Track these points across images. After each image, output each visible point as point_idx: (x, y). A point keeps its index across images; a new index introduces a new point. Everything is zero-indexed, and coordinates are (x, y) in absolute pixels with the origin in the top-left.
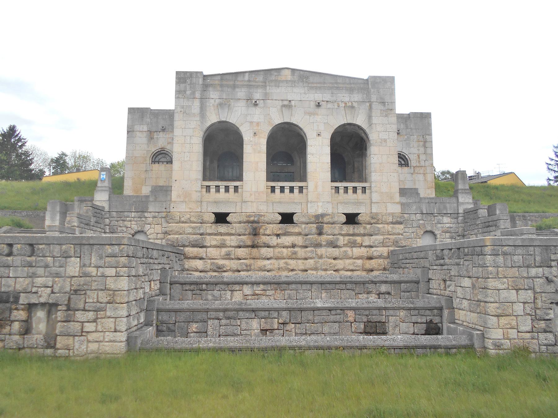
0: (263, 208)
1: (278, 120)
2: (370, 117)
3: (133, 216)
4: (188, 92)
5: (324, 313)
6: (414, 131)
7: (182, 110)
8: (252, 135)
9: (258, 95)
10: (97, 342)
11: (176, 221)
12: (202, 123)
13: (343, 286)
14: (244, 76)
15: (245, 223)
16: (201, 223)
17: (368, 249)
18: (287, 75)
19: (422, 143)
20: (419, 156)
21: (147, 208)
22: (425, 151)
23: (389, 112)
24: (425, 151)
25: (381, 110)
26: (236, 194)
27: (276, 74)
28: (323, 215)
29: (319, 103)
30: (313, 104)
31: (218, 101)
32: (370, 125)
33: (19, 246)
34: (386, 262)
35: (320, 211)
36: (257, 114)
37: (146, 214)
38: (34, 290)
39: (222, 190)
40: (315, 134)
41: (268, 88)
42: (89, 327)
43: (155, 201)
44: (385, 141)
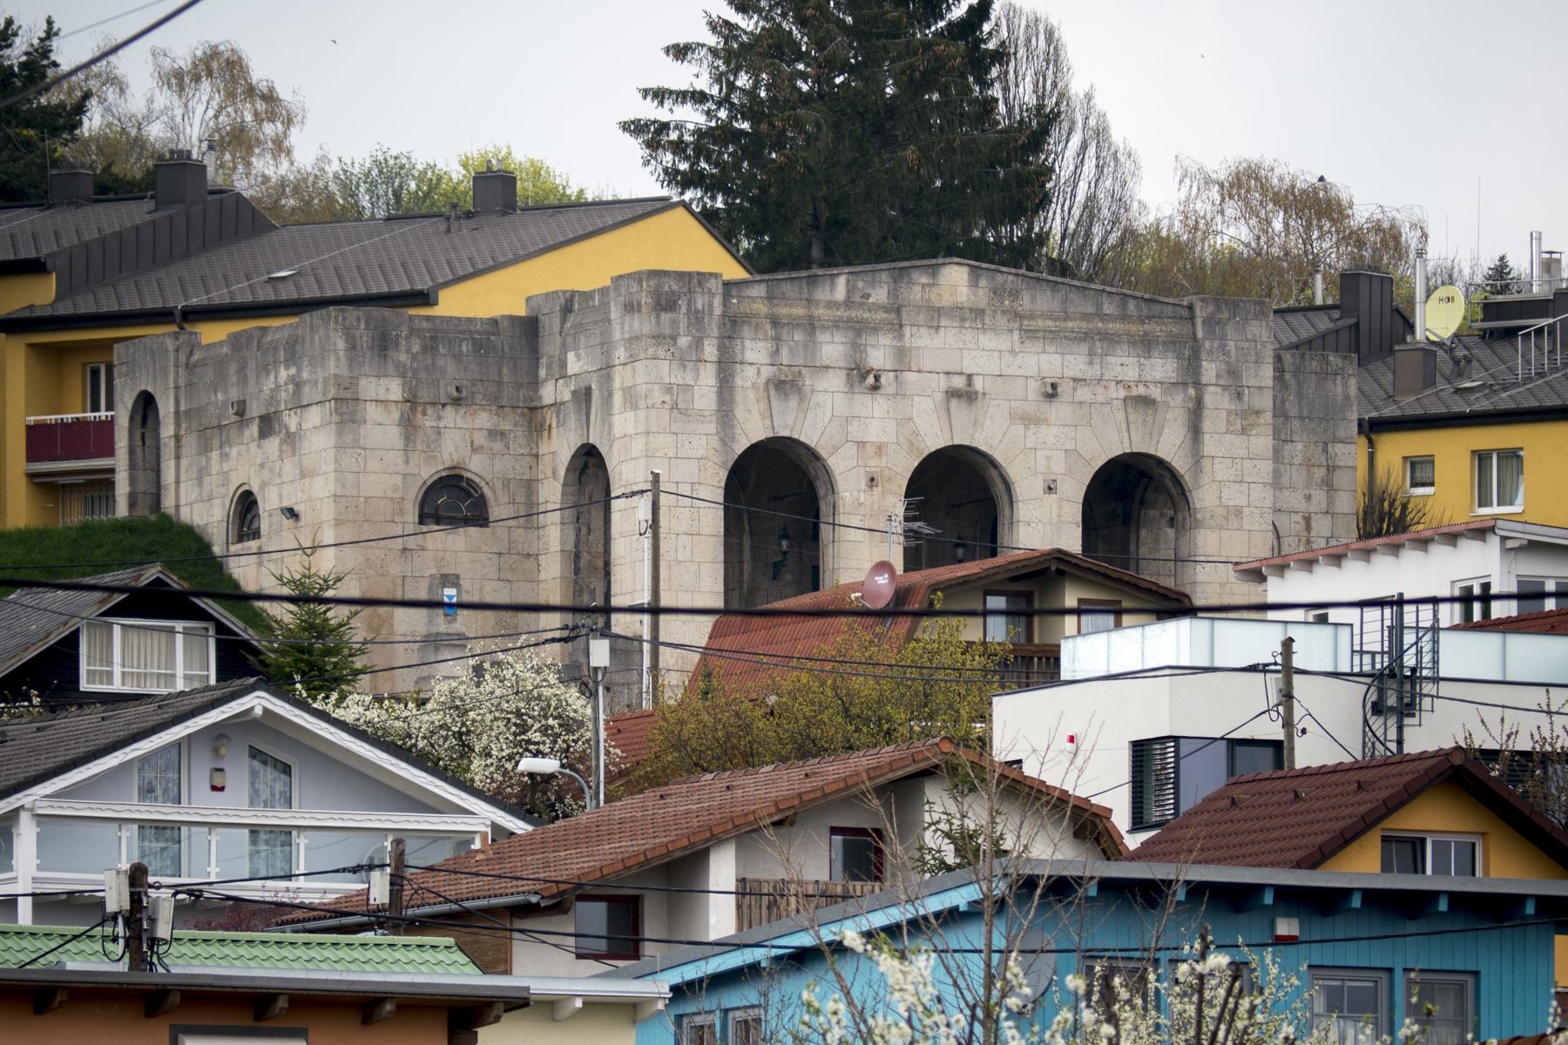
1: (935, 439)
2: (1195, 430)
4: (683, 341)
6: (1296, 424)
7: (667, 398)
8: (863, 486)
9: (879, 355)
12: (723, 442)
19: (1320, 473)
20: (1307, 520)
22: (1330, 502)
23: (1252, 419)
24: (1330, 502)
25: (1229, 413)
27: (924, 280)
29: (1054, 386)
31: (767, 372)
32: (1197, 457)
36: (876, 419)
40: (1039, 486)
41: (907, 331)
44: (1238, 512)
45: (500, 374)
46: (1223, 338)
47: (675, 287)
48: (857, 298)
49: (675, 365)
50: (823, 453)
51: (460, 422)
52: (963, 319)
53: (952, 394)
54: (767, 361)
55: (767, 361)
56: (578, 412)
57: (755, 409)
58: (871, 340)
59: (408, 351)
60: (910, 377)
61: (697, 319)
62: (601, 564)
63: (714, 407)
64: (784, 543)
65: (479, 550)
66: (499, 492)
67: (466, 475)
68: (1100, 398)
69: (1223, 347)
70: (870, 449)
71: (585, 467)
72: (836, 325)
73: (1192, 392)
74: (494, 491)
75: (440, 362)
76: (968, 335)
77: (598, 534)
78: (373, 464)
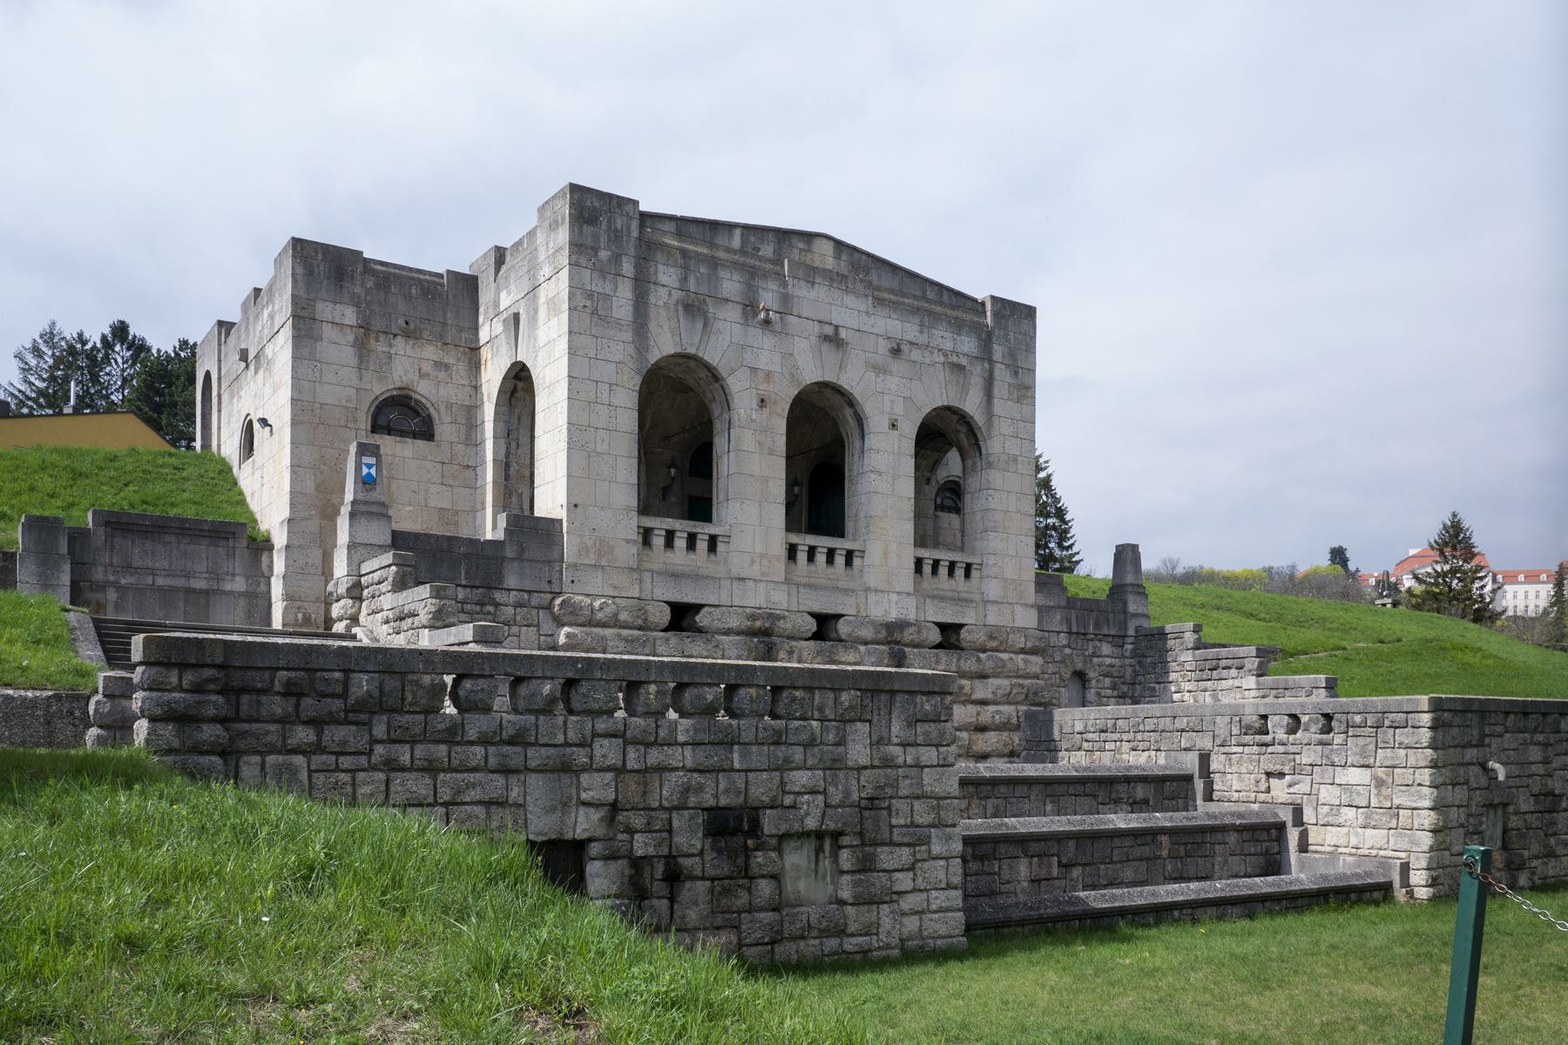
0: (780, 599)
1: (811, 376)
3: (460, 597)
4: (604, 254)
5: (1128, 842)
7: (588, 303)
10: (917, 913)
11: (582, 619)
13: (1080, 789)
14: (731, 235)
15: (738, 633)
16: (640, 628)
17: (979, 708)
18: (824, 257)
21: (501, 578)
26: (712, 557)
27: (801, 245)
28: (902, 625)
30: (884, 346)
31: (677, 295)
32: (990, 415)
33: (753, 691)
34: (1016, 740)
35: (894, 615)
36: (766, 352)
37: (499, 596)
38: (788, 800)
39: (680, 543)
42: (904, 881)
43: (520, 557)
44: (1015, 459)
45: (444, 317)
46: (1006, 328)
47: (597, 204)
48: (749, 249)
49: (596, 275)
50: (723, 372)
51: (409, 352)
52: (832, 280)
53: (826, 338)
54: (676, 285)
55: (676, 285)
56: (508, 337)
57: (666, 326)
58: (762, 283)
59: (363, 285)
60: (792, 320)
61: (617, 237)
62: (527, 474)
63: (630, 318)
64: (673, 471)
65: (425, 458)
66: (443, 413)
67: (414, 396)
68: (928, 361)
69: (1006, 335)
70: (761, 376)
71: (514, 391)
72: (735, 266)
73: (987, 365)
74: (438, 411)
75: (392, 299)
76: (836, 293)
77: (525, 449)
78: (328, 376)
